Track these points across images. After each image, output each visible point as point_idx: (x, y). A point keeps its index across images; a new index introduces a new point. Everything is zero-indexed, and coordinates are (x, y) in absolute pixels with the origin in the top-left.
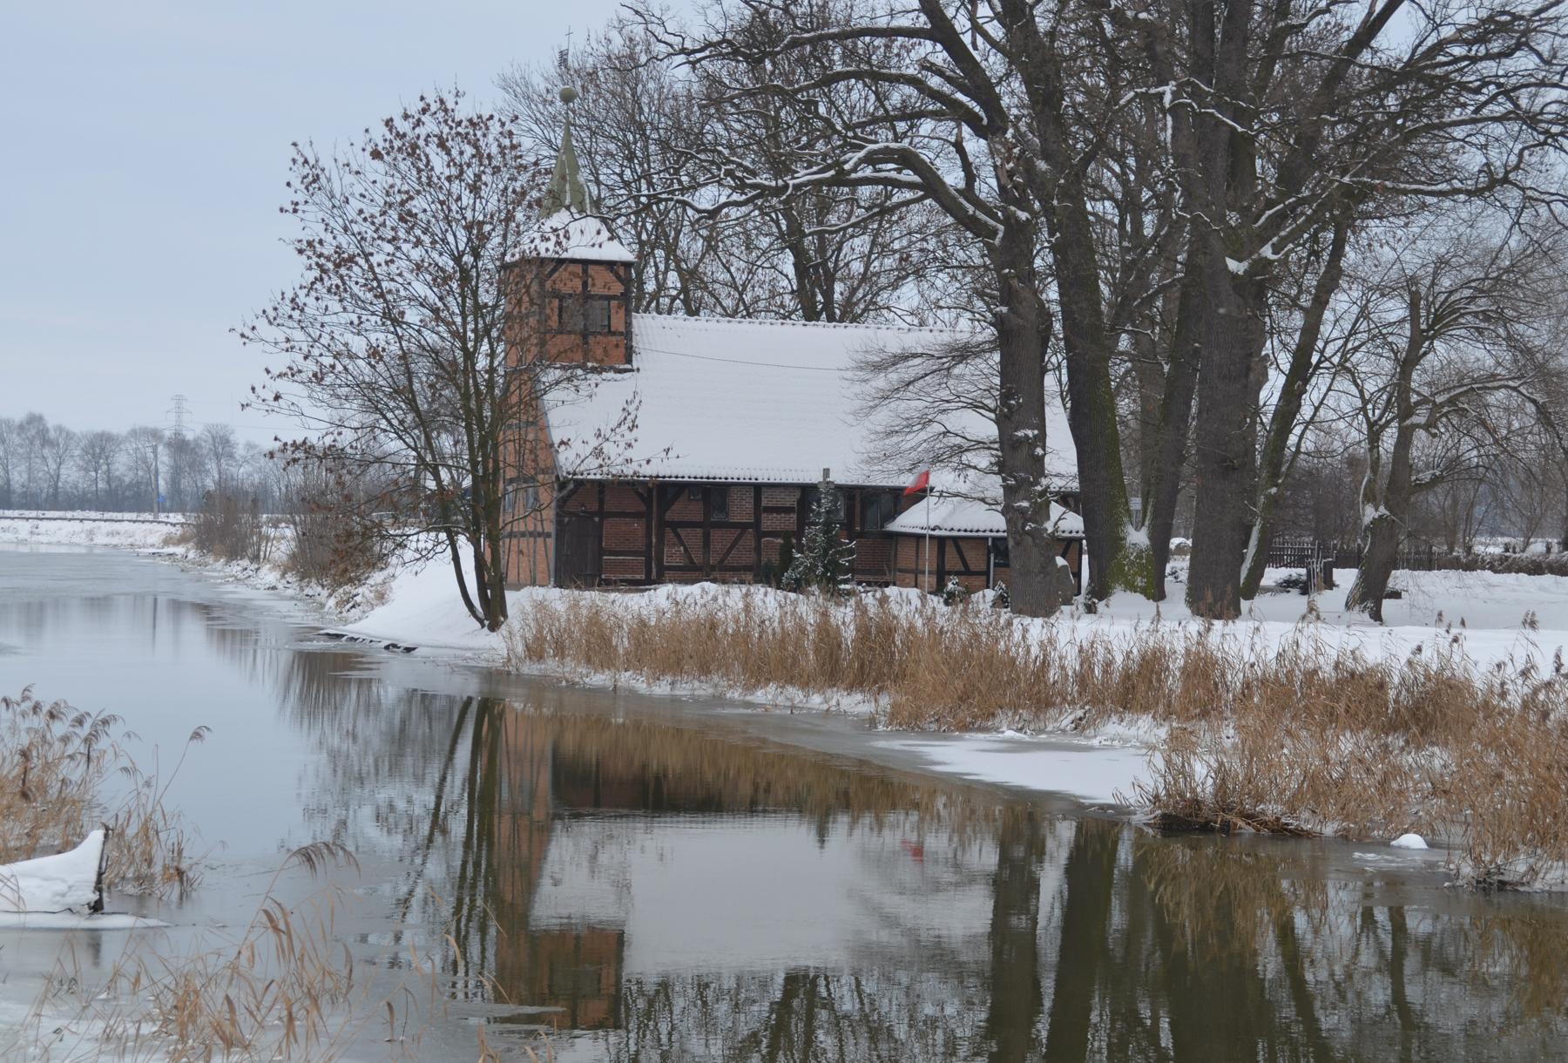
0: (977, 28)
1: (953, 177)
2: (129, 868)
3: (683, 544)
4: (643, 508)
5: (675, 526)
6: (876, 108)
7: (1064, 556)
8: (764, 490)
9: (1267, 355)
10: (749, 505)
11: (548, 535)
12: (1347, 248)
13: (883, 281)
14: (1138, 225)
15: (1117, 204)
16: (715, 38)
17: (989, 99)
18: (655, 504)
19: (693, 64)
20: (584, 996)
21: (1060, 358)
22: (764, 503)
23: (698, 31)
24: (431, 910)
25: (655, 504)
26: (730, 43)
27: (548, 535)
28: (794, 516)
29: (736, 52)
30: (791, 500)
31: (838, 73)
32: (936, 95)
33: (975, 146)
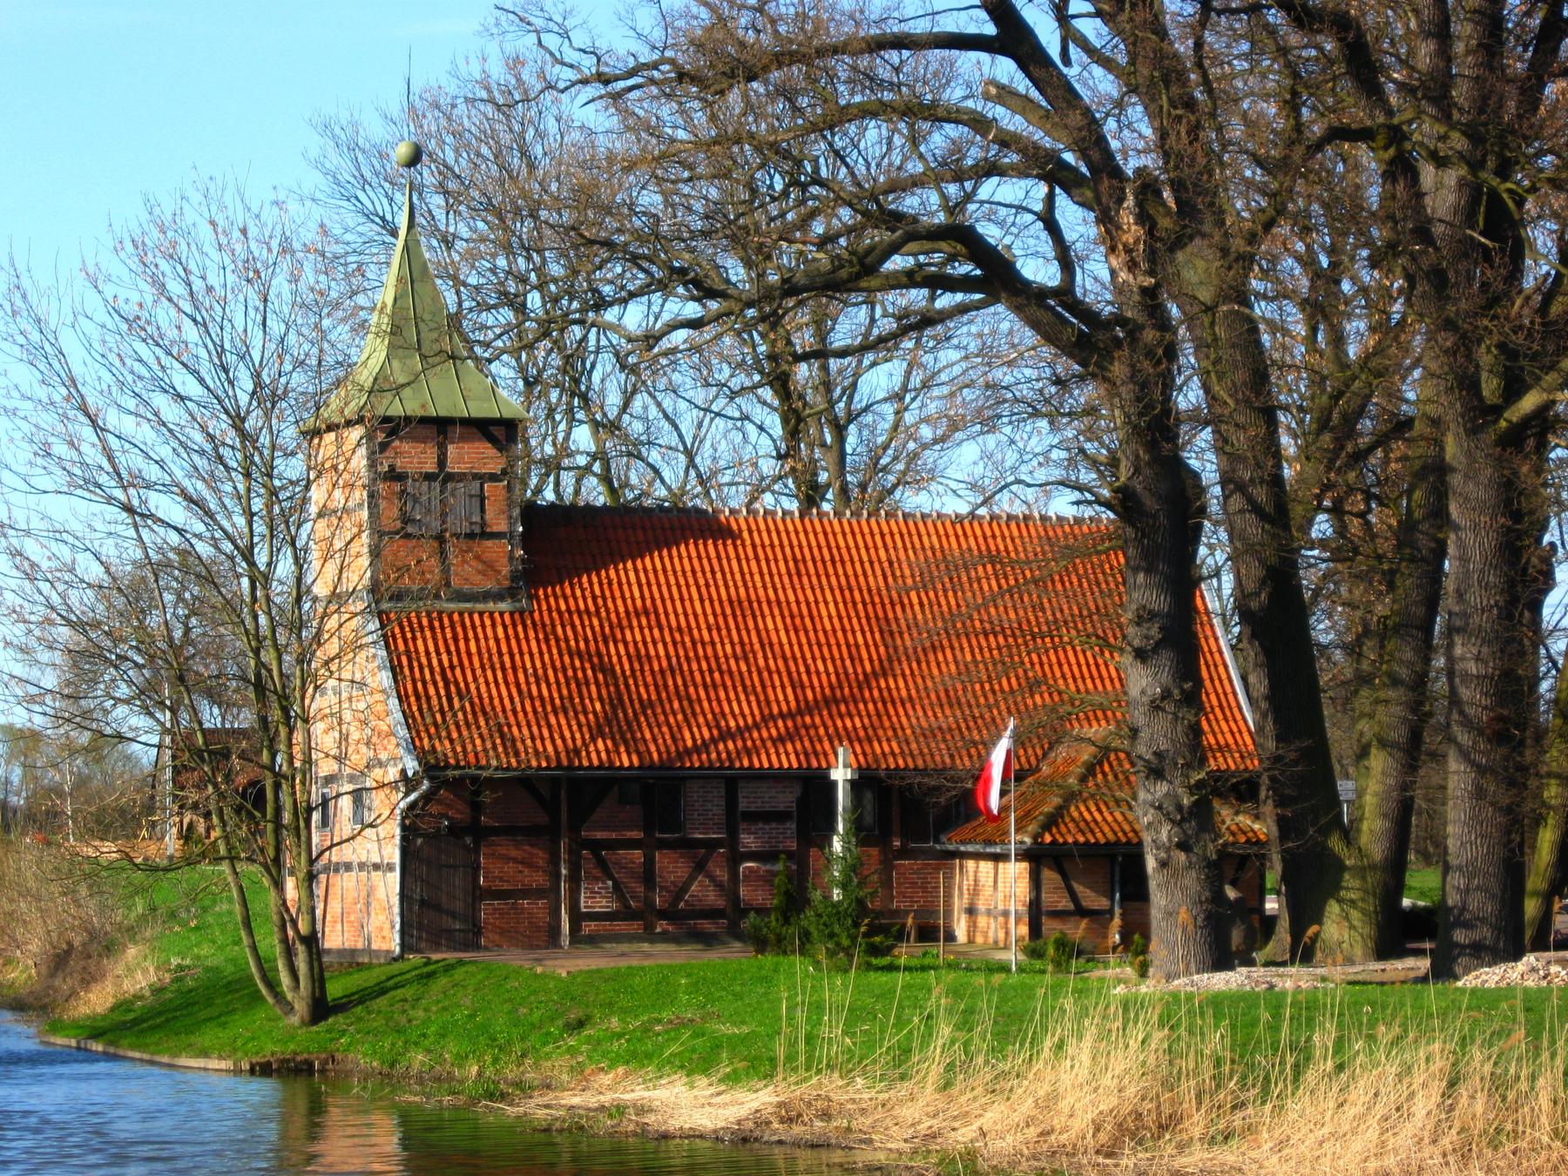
0: (1069, 35)
1: (1039, 270)
2: (279, 885)
3: (611, 877)
4: (542, 819)
5: (595, 845)
6: (905, 159)
7: (1234, 884)
8: (741, 784)
9: (1552, 545)
10: (717, 808)
11: (390, 868)
12: (1333, 908)
13: (926, 432)
14: (1338, 340)
15: (1304, 304)
16: (646, 56)
17: (1092, 141)
18: (564, 808)
19: (617, 97)
20: (1533, 220)
21: (1210, 561)
22: (743, 805)
23: (623, 46)
24: (707, 926)
25: (564, 808)
26: (672, 62)
27: (390, 868)
28: (792, 826)
29: (682, 76)
30: (786, 799)
31: (371, 515)
32: (1007, 141)
33: (1074, 219)
